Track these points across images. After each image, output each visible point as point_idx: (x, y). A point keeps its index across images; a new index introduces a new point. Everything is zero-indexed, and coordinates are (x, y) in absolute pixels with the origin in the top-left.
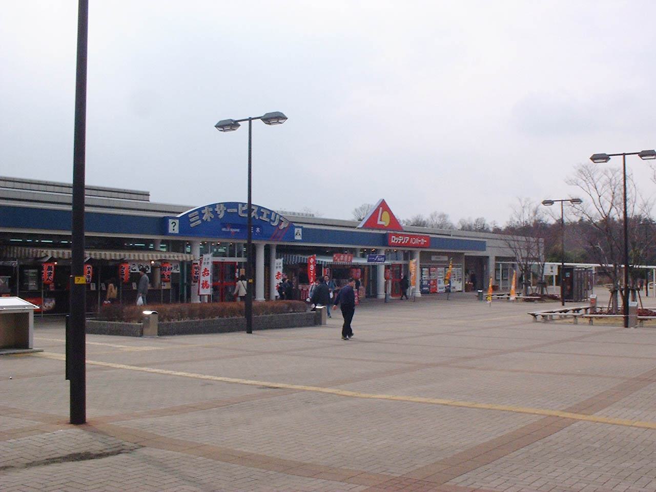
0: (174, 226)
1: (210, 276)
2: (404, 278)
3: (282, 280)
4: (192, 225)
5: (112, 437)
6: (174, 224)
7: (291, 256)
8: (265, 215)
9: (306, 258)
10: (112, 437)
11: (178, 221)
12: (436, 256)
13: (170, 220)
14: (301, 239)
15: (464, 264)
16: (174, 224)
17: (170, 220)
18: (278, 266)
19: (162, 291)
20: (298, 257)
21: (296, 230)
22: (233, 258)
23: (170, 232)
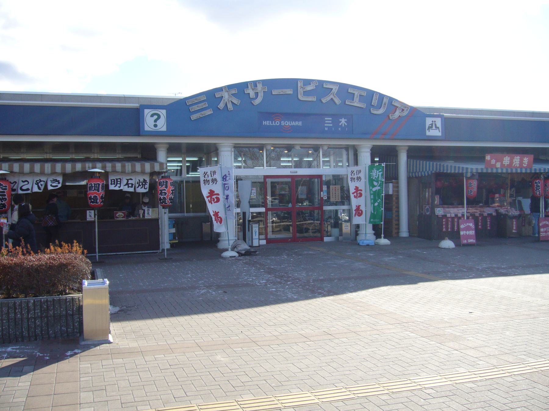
0: (156, 121)
1: (363, 197)
2: (273, 122)
3: (59, 295)
4: (194, 117)
5: (460, 318)
6: (156, 117)
7: (418, 161)
8: (356, 99)
9: (449, 165)
10: (460, 318)
11: (164, 112)
12: (243, 257)
13: (146, 111)
14: (439, 134)
15: (150, 217)
16: (156, 117)
17: (146, 111)
18: (355, 177)
19: (166, 251)
20: (440, 165)
21: (429, 121)
22: (291, 169)
23: (147, 128)
